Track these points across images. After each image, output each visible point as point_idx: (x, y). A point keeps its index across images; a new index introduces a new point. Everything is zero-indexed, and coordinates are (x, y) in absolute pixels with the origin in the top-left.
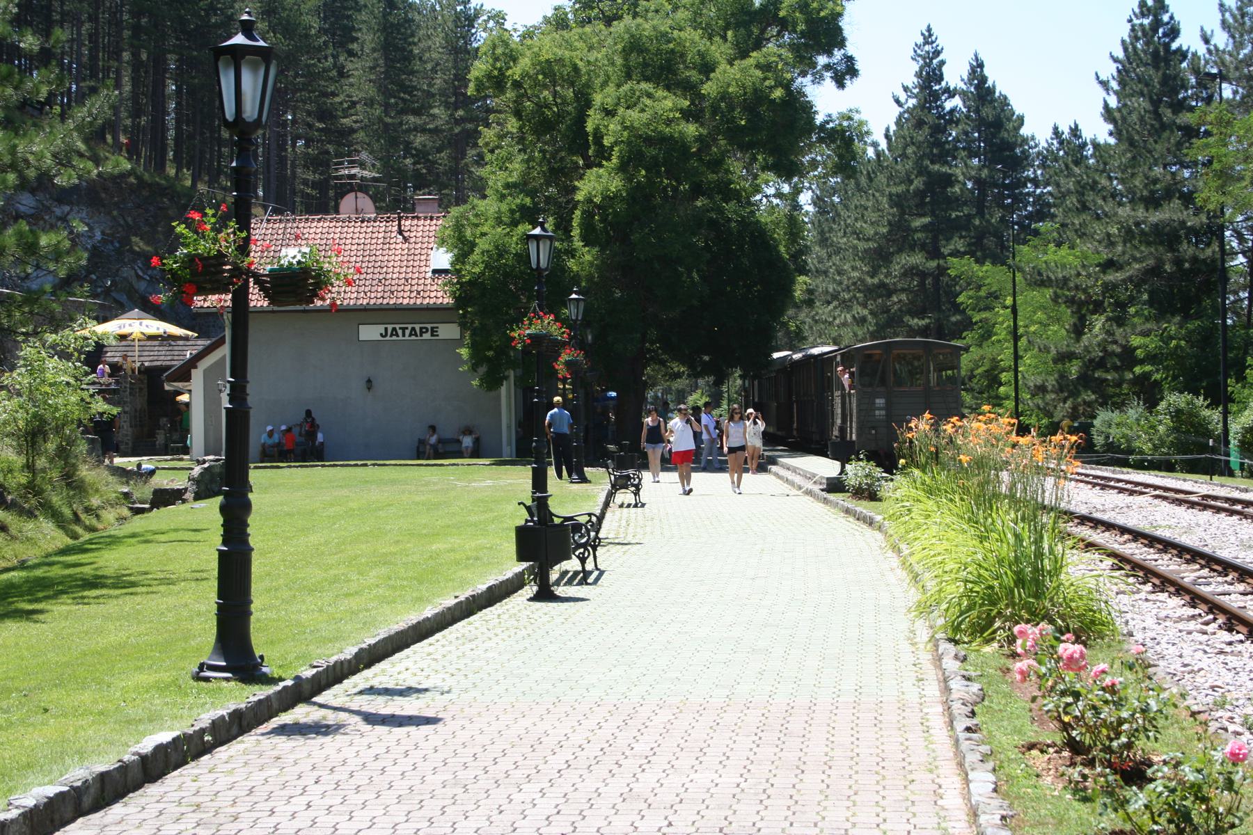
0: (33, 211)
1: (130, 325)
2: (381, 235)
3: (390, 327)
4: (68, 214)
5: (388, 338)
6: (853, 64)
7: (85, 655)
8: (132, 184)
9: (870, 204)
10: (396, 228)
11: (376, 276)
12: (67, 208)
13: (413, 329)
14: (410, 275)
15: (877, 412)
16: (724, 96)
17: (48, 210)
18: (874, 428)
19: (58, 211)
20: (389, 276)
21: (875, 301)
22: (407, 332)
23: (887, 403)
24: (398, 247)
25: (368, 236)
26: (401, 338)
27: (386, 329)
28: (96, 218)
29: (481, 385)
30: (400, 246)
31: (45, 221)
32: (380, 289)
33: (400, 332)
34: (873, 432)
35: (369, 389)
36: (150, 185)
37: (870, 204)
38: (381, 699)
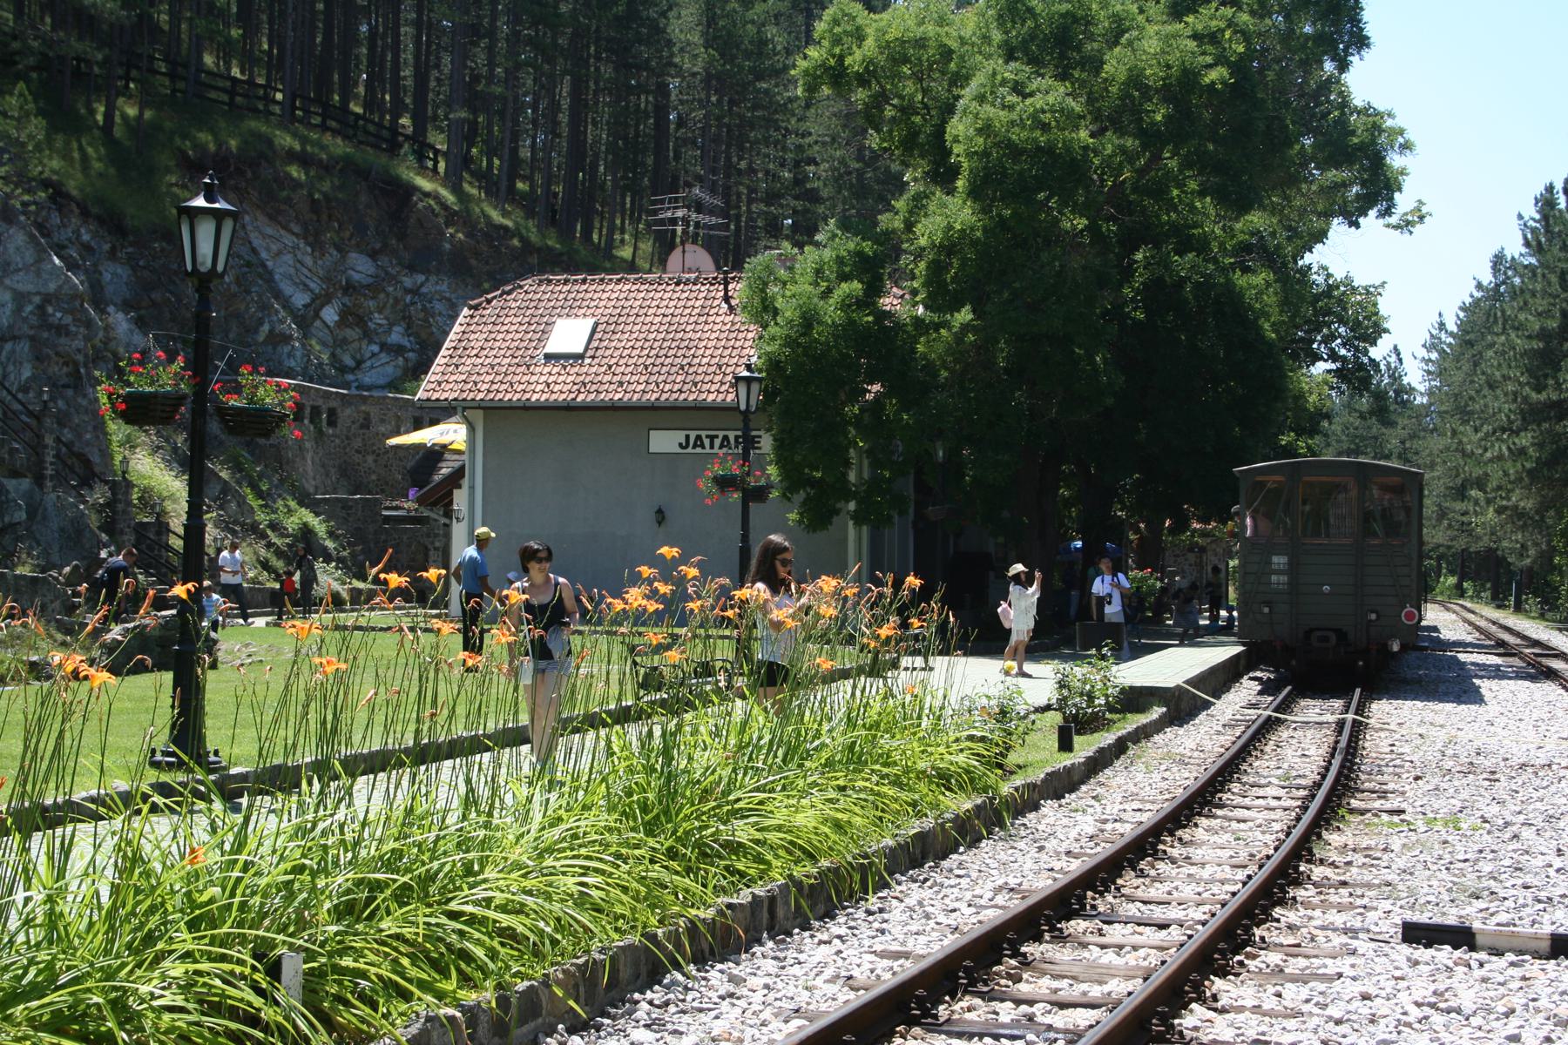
0: (371, 280)
1: (455, 431)
2: (698, 303)
3: (693, 435)
4: (422, 285)
5: (689, 450)
6: (1362, 30)
7: (468, 871)
8: (514, 248)
9: (1538, 287)
10: (722, 294)
11: (678, 361)
12: (421, 278)
13: (726, 438)
14: (725, 360)
15: (1274, 578)
16: (1135, 79)
17: (393, 279)
18: (1268, 603)
19: (408, 282)
20: (696, 361)
21: (1539, 425)
22: (717, 442)
23: (1290, 563)
24: (719, 319)
25: (681, 303)
26: (708, 450)
27: (687, 437)
28: (460, 292)
29: (800, 522)
30: (721, 319)
31: (388, 295)
32: (679, 379)
33: (707, 442)
34: (1266, 610)
35: (660, 523)
36: (539, 250)
37: (1538, 287)
38: (933, 945)
